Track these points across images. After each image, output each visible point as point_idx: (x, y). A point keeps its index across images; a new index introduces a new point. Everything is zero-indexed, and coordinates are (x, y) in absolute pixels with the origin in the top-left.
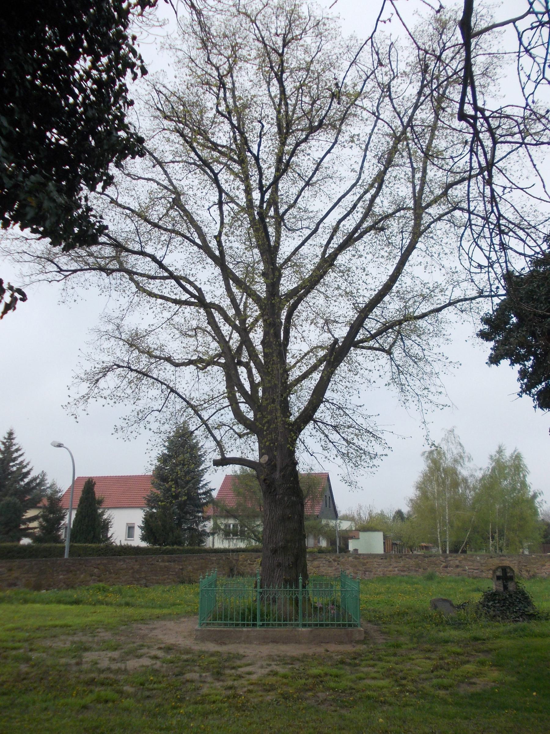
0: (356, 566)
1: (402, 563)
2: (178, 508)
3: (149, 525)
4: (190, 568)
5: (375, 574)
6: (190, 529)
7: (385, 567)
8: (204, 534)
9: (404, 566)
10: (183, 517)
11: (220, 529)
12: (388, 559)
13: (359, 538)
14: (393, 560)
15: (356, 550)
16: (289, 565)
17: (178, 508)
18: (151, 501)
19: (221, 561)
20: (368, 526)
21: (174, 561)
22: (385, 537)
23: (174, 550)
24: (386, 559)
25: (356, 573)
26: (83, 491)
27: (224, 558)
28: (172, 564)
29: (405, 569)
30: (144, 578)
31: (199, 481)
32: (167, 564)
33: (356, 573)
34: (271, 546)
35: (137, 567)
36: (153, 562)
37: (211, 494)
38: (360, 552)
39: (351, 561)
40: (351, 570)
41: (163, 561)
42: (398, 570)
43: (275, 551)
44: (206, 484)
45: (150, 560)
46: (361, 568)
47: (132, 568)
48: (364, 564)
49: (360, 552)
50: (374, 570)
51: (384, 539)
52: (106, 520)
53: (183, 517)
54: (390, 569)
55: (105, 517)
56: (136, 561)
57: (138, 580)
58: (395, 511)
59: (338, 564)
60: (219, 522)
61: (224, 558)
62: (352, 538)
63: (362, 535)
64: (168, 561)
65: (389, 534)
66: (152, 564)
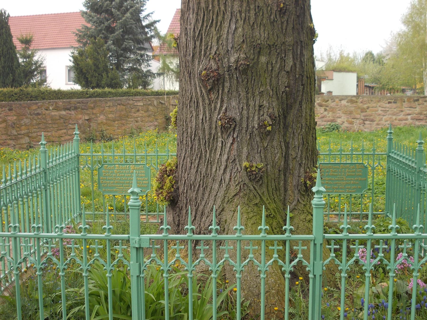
0: (351, 113)
1: (418, 110)
2: (113, 44)
3: (78, 65)
4: (102, 118)
5: (378, 124)
6: (131, 69)
7: (393, 114)
8: (150, 74)
9: (420, 114)
10: (121, 56)
11: (169, 69)
12: (399, 104)
13: (333, 80)
14: (405, 104)
15: (330, 92)
16: (262, 126)
17: (113, 44)
18: (84, 36)
19: (151, 108)
20: (341, 67)
21: (76, 108)
22: (359, 79)
23: (105, 93)
24: (395, 102)
25: (351, 123)
26: (10, 29)
27: (155, 103)
28: (73, 112)
29: (422, 117)
30: (27, 135)
31: (140, 11)
32: (63, 113)
33: (351, 123)
34: (199, 67)
35: (12, 118)
36: (39, 111)
37: (155, 29)
38: (334, 94)
39: (345, 106)
40: (344, 118)
41: (57, 109)
42: (412, 119)
43: (214, 82)
44: (148, 15)
45: (34, 107)
46: (358, 116)
47: (5, 121)
48: (363, 110)
49: (334, 94)
50: (378, 118)
51: (358, 82)
52: (37, 62)
53: (121, 56)
54: (401, 116)
55: (35, 58)
56: (10, 110)
57: (16, 138)
58: (365, 52)
59: (326, 110)
60: (168, 61)
61: (155, 103)
62: (324, 79)
63: (336, 75)
64: (66, 109)
65: (362, 75)
66: (38, 114)
